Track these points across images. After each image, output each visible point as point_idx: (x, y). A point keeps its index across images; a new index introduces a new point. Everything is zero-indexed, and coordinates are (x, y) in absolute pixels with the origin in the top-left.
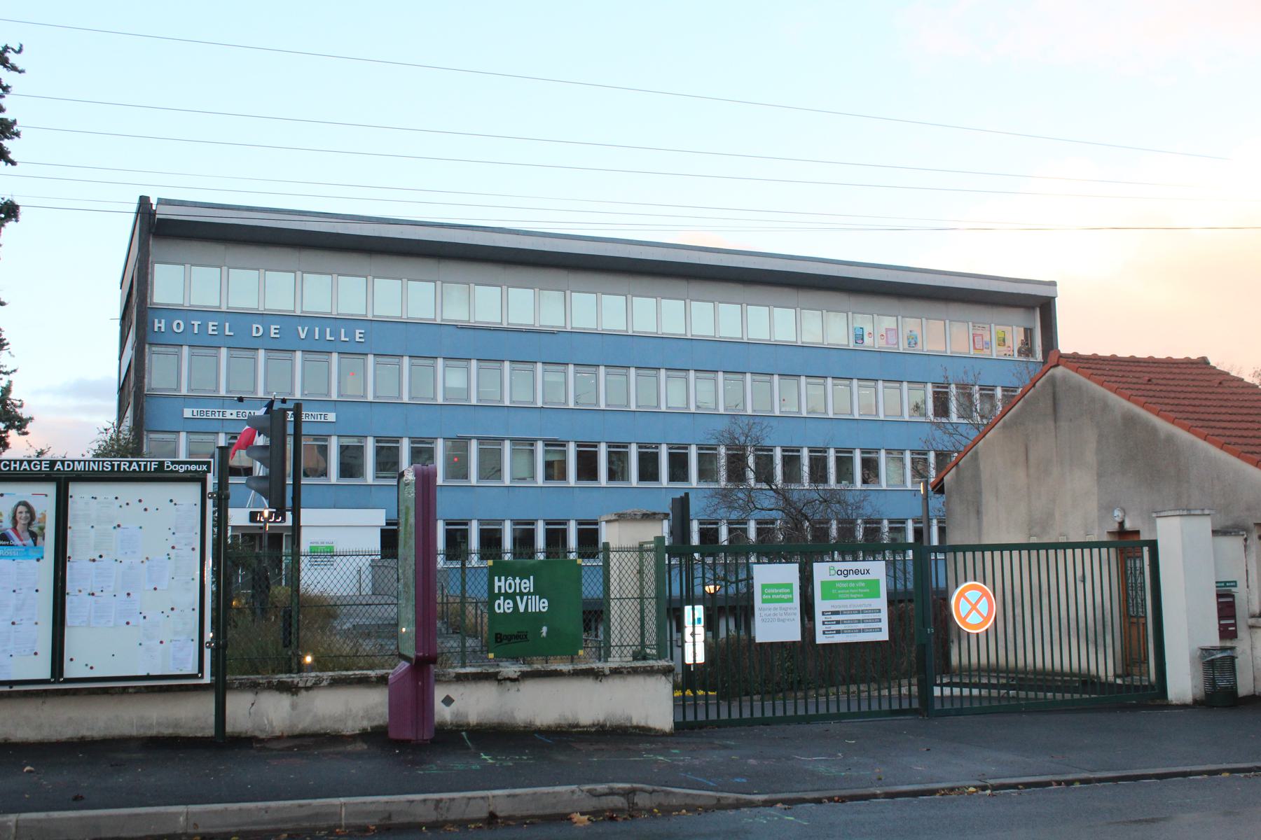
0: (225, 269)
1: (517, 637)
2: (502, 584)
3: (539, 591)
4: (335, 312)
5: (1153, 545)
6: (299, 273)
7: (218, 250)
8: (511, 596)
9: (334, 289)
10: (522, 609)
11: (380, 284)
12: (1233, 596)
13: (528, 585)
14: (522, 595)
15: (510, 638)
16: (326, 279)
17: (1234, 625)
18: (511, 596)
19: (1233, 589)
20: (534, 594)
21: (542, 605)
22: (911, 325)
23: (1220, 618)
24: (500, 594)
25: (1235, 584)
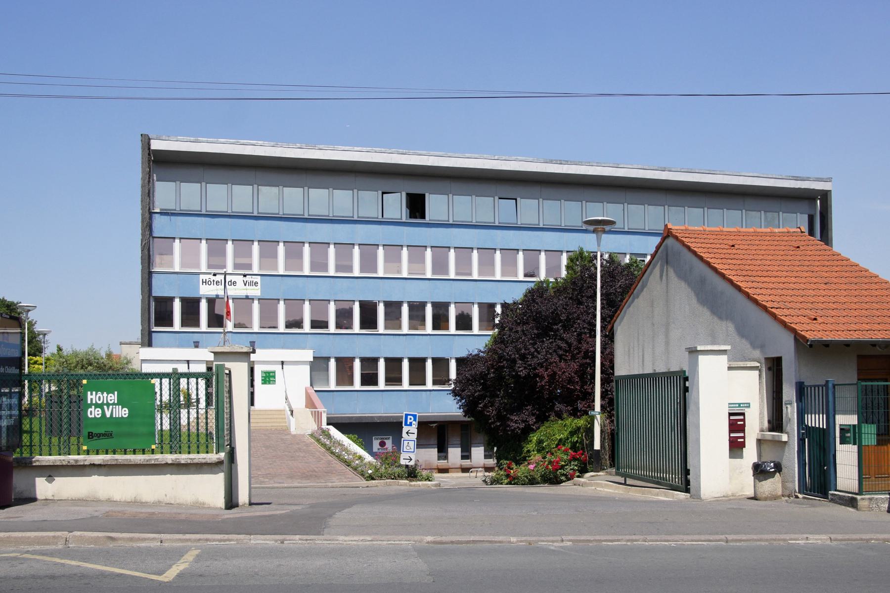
0: (204, 184)
1: (104, 435)
2: (93, 397)
3: (121, 402)
4: (281, 213)
5: (229, 374)
6: (355, 191)
7: (199, 172)
8: (101, 406)
9: (231, 194)
10: (108, 415)
11: (264, 189)
12: (743, 414)
13: (113, 398)
14: (108, 405)
15: (99, 436)
16: (223, 187)
17: (744, 437)
18: (101, 406)
19: (746, 409)
20: (118, 404)
21: (123, 412)
22: (715, 214)
23: (731, 431)
24: (92, 404)
25: (748, 405)
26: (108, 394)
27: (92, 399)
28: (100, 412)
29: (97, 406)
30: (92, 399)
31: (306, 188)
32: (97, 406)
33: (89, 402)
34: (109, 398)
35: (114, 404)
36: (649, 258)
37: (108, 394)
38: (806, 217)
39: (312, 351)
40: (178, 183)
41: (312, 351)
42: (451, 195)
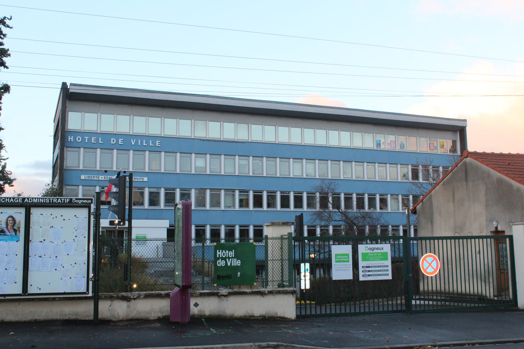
0: (99, 114)
1: (227, 277)
3: (237, 257)
6: (132, 116)
7: (96, 106)
8: (224, 259)
10: (229, 264)
14: (229, 258)
15: (223, 277)
16: (174, 121)
18: (224, 259)
20: (235, 258)
22: (402, 139)
24: (219, 258)
26: (229, 251)
27: (219, 255)
28: (224, 263)
29: (222, 259)
30: (219, 255)
31: (163, 118)
32: (222, 259)
33: (218, 256)
34: (229, 254)
35: (232, 258)
36: (450, 168)
37: (229, 251)
38: (451, 141)
39: (168, 221)
40: (115, 115)
41: (168, 221)
42: (250, 125)
